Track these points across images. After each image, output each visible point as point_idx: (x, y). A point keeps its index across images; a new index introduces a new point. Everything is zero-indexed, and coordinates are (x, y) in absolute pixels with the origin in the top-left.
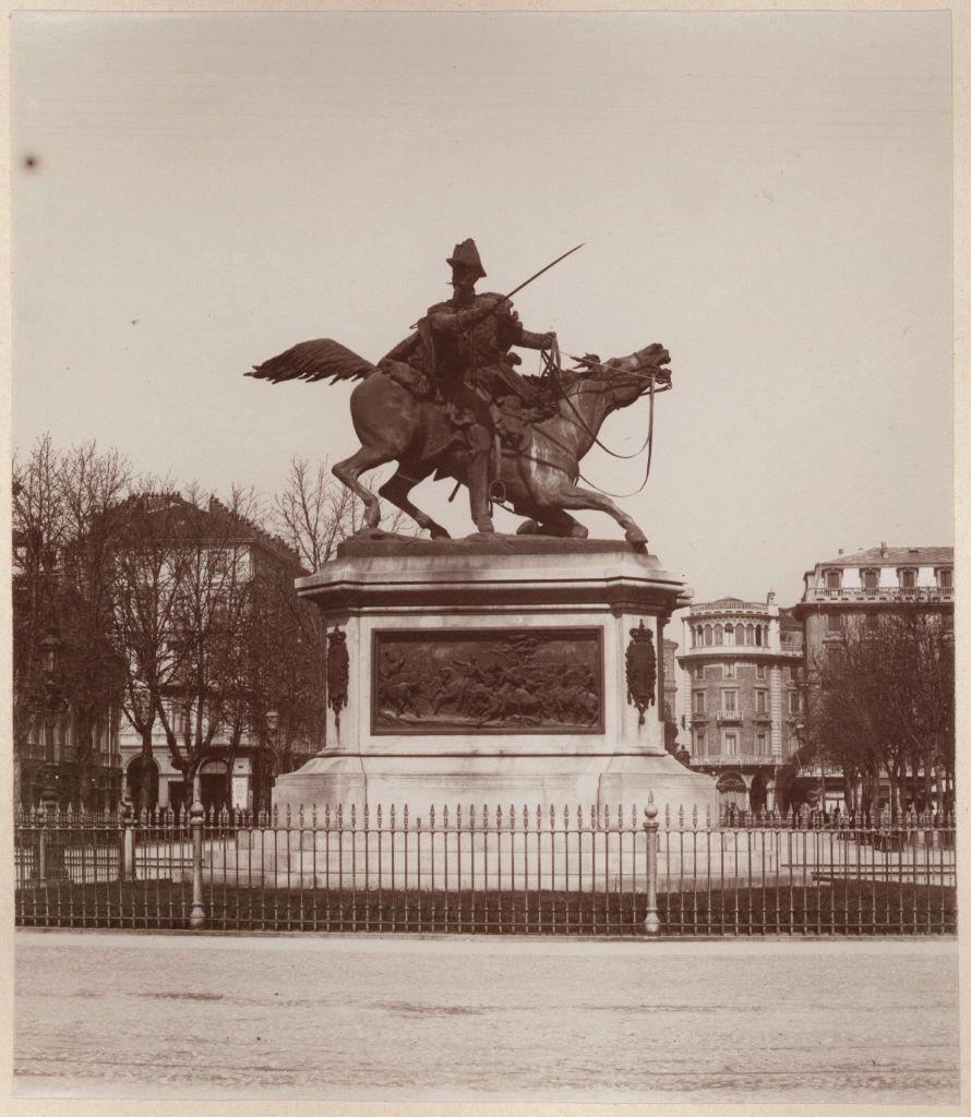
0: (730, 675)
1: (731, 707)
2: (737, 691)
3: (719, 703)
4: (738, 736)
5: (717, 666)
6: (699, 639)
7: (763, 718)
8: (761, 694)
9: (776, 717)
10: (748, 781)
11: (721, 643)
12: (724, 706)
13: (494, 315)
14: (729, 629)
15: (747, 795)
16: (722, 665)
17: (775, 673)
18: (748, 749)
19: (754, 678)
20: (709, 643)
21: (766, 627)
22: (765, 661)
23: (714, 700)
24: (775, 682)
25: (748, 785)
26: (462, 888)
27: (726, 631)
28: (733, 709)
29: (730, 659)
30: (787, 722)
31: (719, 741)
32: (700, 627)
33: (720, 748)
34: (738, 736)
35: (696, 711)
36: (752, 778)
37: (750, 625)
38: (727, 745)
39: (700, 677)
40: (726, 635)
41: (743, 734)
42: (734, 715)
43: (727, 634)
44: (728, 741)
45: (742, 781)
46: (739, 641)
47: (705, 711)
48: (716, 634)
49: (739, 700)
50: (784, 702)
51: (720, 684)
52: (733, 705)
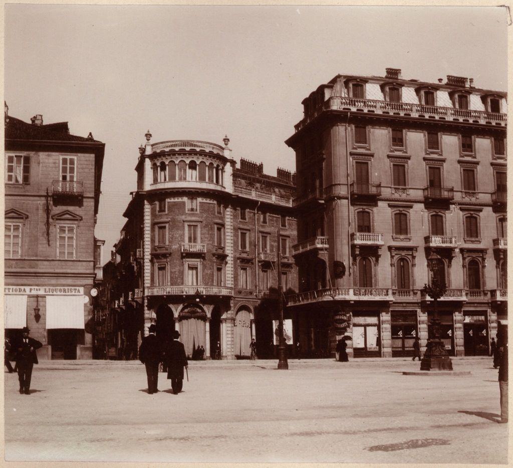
0: (192, 210)
1: (192, 239)
2: (199, 224)
3: (183, 235)
4: (200, 267)
5: (180, 200)
6: (161, 175)
7: (220, 251)
8: (219, 229)
9: (229, 250)
10: (208, 311)
11: (185, 179)
12: (187, 239)
13: (50, 196)
14: (193, 166)
15: (208, 324)
16: (185, 199)
17: (229, 212)
18: (208, 281)
19: (214, 214)
20: (172, 178)
21: (223, 168)
22: (223, 199)
23: (177, 234)
24: (229, 220)
25: (209, 315)
26: (242, 355)
27: (190, 168)
28: (195, 242)
29: (192, 194)
30: (238, 258)
31: (182, 273)
32: (163, 164)
33: (183, 279)
34: (200, 267)
35: (157, 244)
36: (211, 307)
37: (211, 164)
38: (189, 276)
39: (162, 210)
40: (189, 172)
41: (204, 267)
42: (197, 247)
43: (191, 170)
44: (190, 272)
45: (203, 311)
46: (202, 178)
47: (167, 243)
48: (180, 170)
49: (201, 234)
50: (235, 239)
51: (183, 217)
52: (195, 239)
